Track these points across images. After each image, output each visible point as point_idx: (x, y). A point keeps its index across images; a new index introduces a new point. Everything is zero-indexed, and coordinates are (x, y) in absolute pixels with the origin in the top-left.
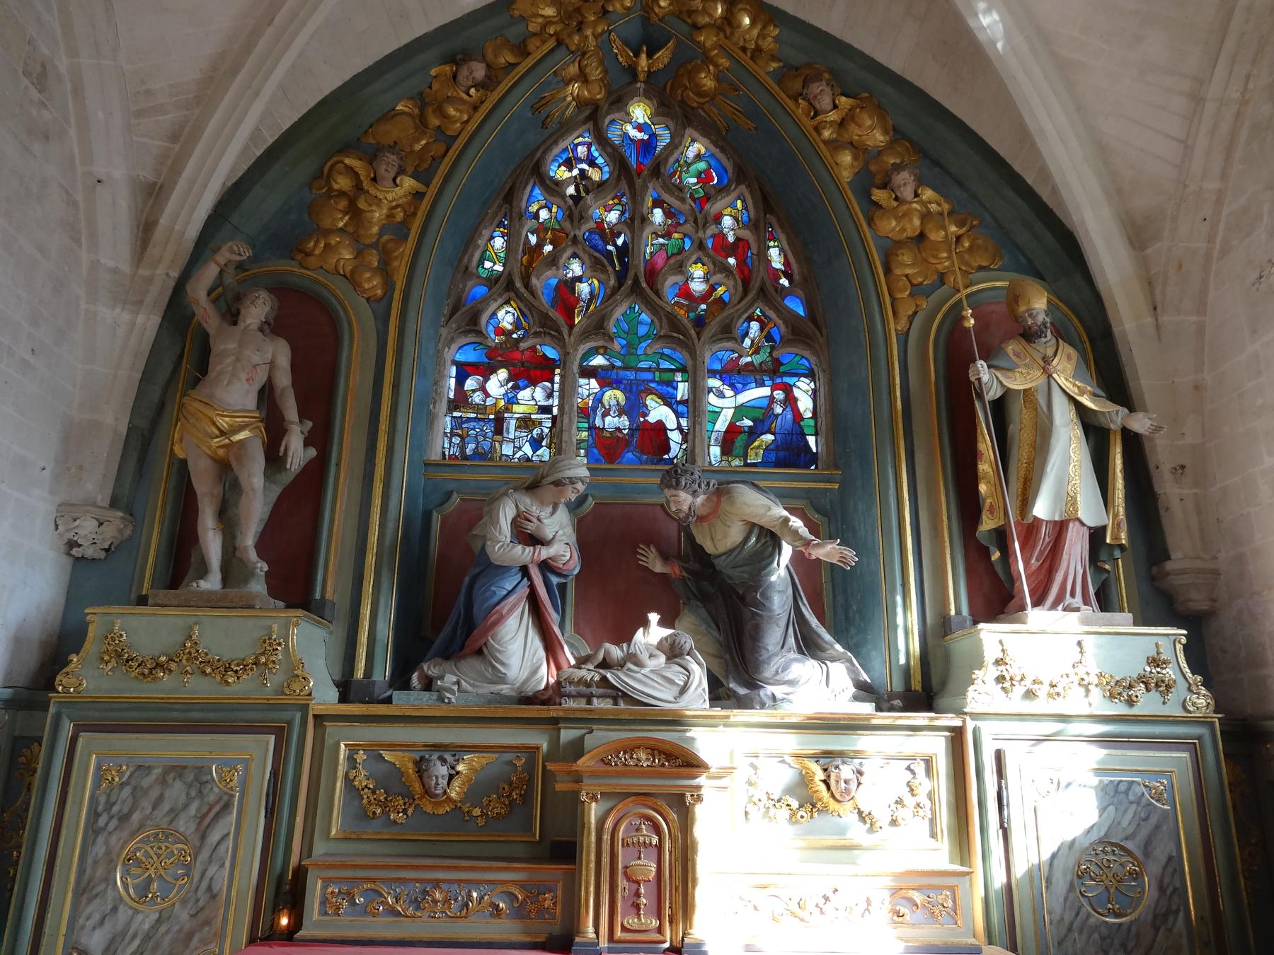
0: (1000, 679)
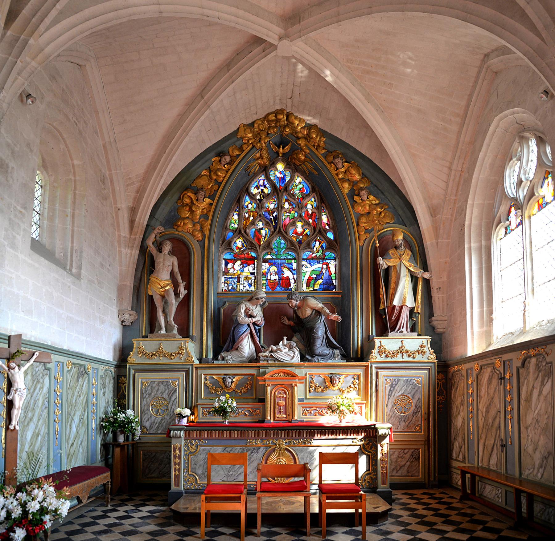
0: (379, 352)
